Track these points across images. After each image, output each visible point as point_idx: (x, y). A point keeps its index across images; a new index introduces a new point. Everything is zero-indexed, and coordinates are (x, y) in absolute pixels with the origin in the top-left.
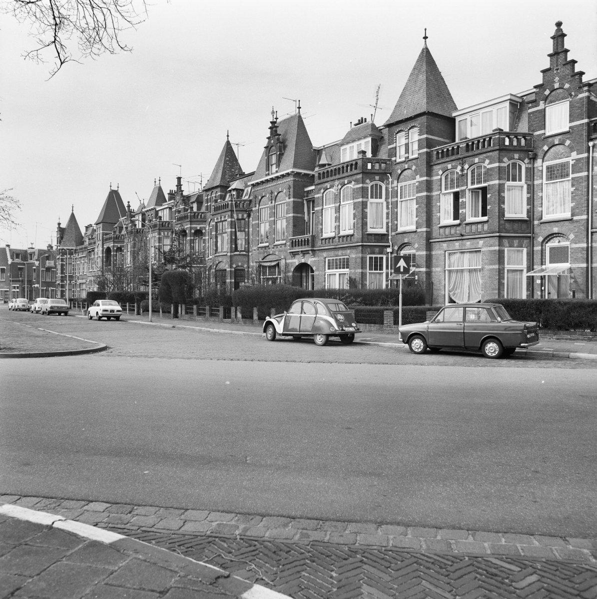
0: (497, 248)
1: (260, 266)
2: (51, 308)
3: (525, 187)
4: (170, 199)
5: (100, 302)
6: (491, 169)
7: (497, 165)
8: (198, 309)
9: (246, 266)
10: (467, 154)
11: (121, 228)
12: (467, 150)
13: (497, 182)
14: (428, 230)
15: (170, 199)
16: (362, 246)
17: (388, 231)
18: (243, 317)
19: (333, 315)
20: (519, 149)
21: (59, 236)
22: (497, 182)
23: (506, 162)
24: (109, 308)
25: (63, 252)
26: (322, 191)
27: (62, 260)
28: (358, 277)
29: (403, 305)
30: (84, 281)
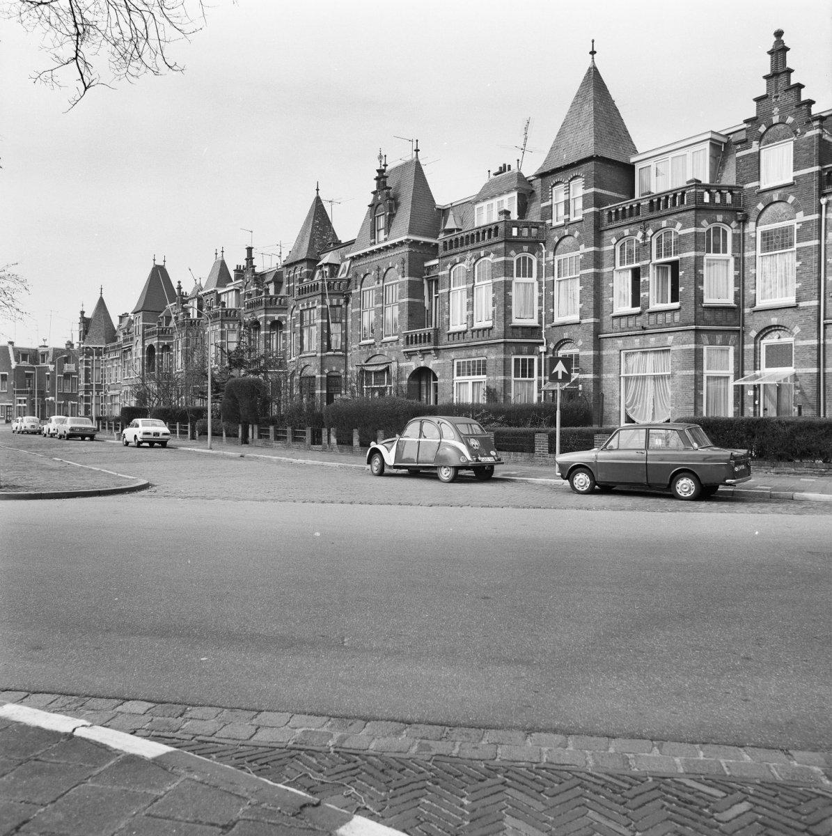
0: (692, 346)
1: (362, 371)
2: (72, 429)
3: (732, 260)
4: (237, 278)
6: (685, 236)
7: (692, 230)
8: (276, 431)
9: (342, 371)
10: (651, 216)
11: (169, 319)
12: (651, 210)
13: (692, 254)
14: (597, 321)
15: (237, 278)
16: (504, 343)
17: (540, 322)
18: (339, 443)
19: (465, 439)
20: (723, 208)
21: (82, 329)
22: (692, 254)
23: (705, 226)
24: (152, 429)
25: (88, 352)
26: (449, 266)
28: (499, 387)
29: (562, 425)
30: (117, 392)
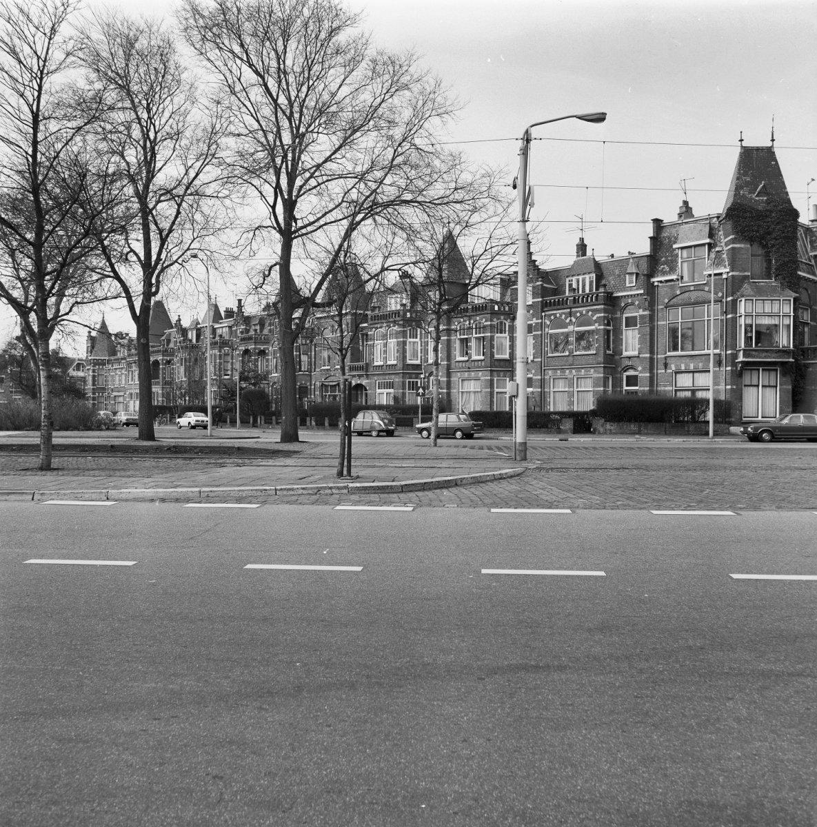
0: (489, 378)
1: (322, 384)
2: (127, 420)
3: (508, 337)
4: (227, 317)
5: (191, 414)
6: (487, 326)
7: (489, 323)
8: (277, 419)
9: (308, 384)
10: (472, 314)
11: (169, 341)
12: (473, 311)
13: (489, 334)
14: (449, 363)
15: (227, 317)
16: (403, 373)
17: (421, 362)
18: (317, 425)
19: (382, 420)
20: (504, 313)
21: (90, 345)
22: (489, 334)
23: (495, 322)
24: (200, 419)
25: (97, 363)
26: (374, 330)
27: (94, 371)
28: (400, 396)
29: (422, 414)
30: (122, 394)
